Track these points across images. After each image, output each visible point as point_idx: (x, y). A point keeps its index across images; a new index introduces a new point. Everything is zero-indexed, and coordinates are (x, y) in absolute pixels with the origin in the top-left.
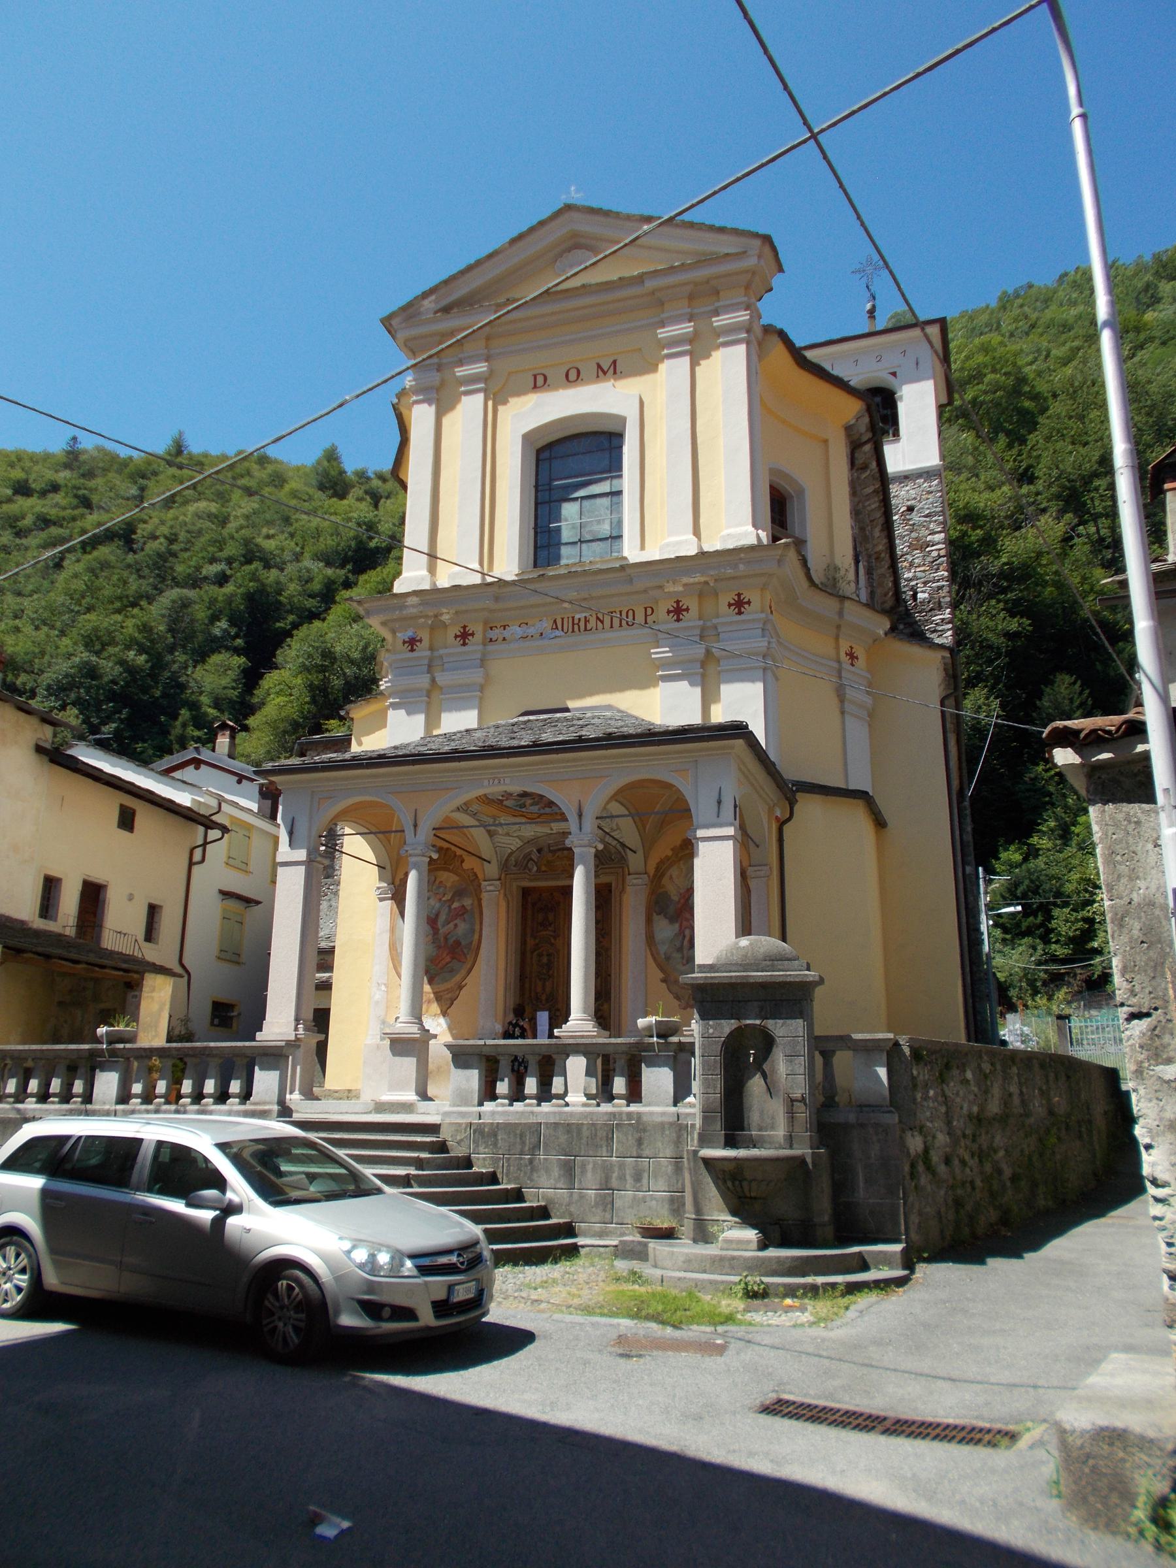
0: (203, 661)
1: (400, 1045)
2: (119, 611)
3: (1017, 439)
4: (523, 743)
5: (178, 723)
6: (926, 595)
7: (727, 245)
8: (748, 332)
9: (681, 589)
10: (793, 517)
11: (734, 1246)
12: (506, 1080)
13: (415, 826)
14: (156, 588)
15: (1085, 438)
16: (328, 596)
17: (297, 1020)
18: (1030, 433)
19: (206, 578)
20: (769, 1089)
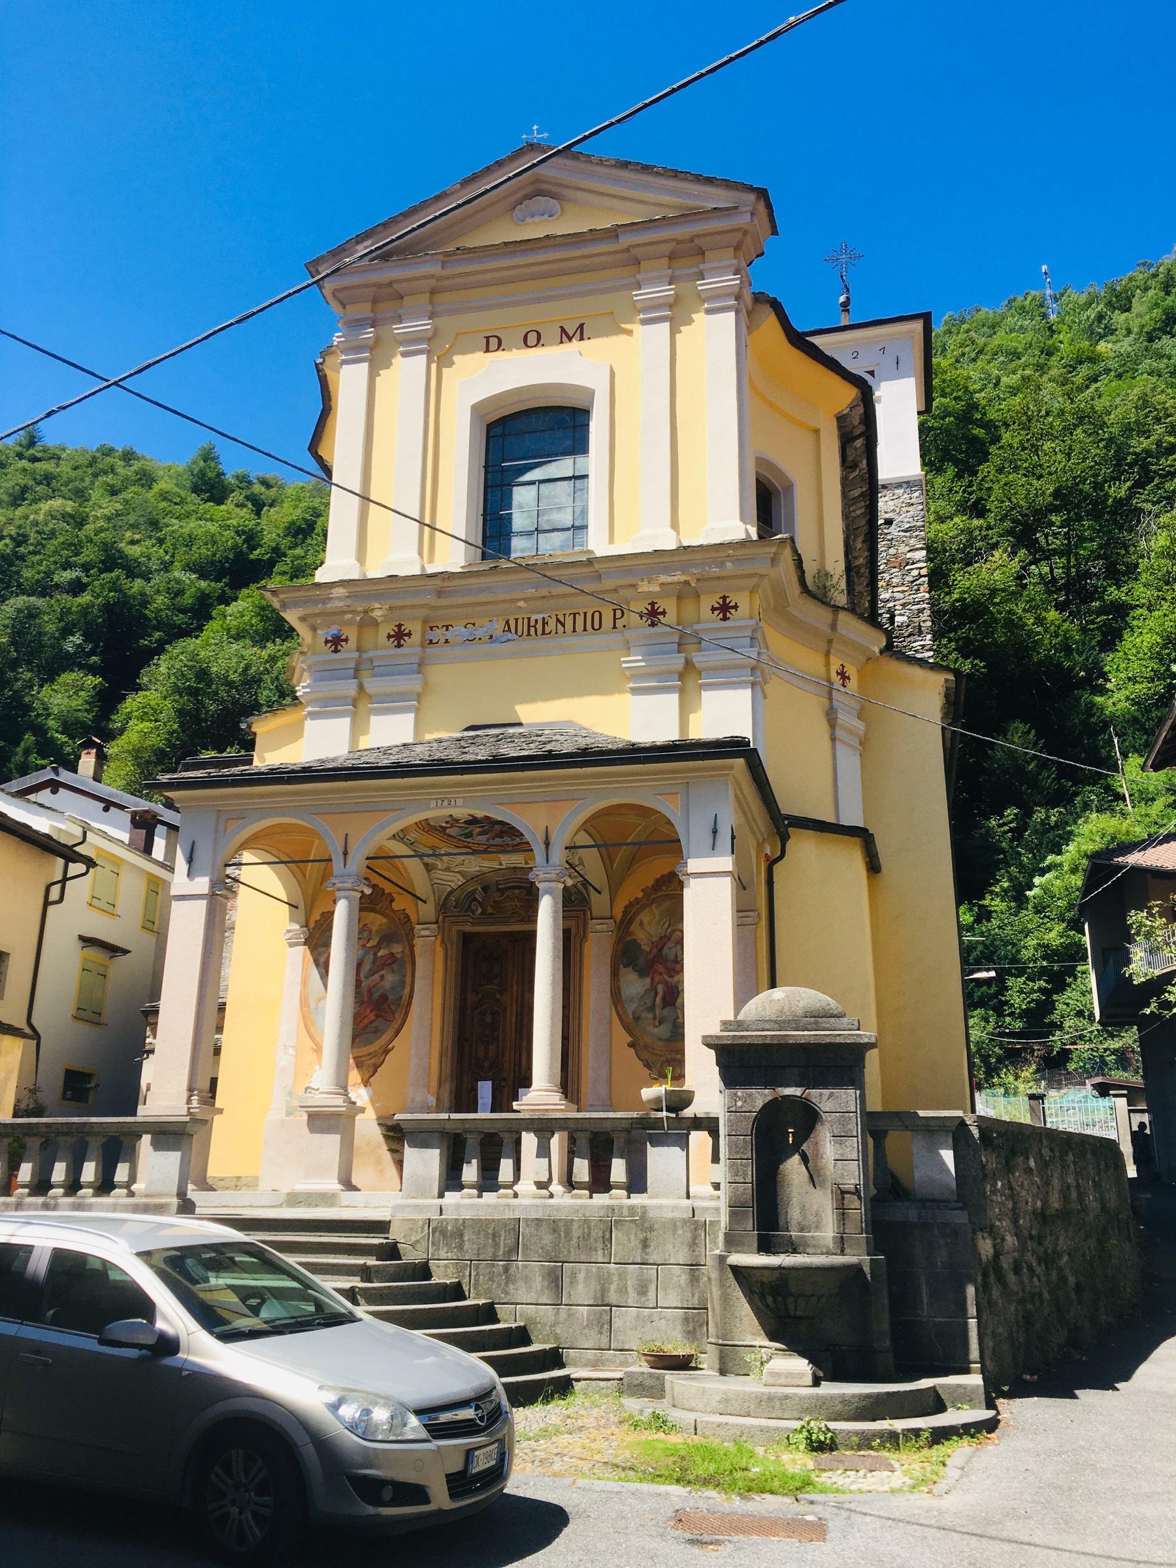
0: (52, 680)
1: (320, 1121)
3: (966, 469)
4: (479, 757)
5: (19, 750)
6: (905, 618)
7: (718, 198)
9: (657, 589)
11: (783, 1381)
12: (474, 1161)
13: (345, 853)
15: (1038, 471)
16: (201, 611)
17: (191, 1090)
18: (980, 464)
19: (57, 586)
20: (811, 1177)
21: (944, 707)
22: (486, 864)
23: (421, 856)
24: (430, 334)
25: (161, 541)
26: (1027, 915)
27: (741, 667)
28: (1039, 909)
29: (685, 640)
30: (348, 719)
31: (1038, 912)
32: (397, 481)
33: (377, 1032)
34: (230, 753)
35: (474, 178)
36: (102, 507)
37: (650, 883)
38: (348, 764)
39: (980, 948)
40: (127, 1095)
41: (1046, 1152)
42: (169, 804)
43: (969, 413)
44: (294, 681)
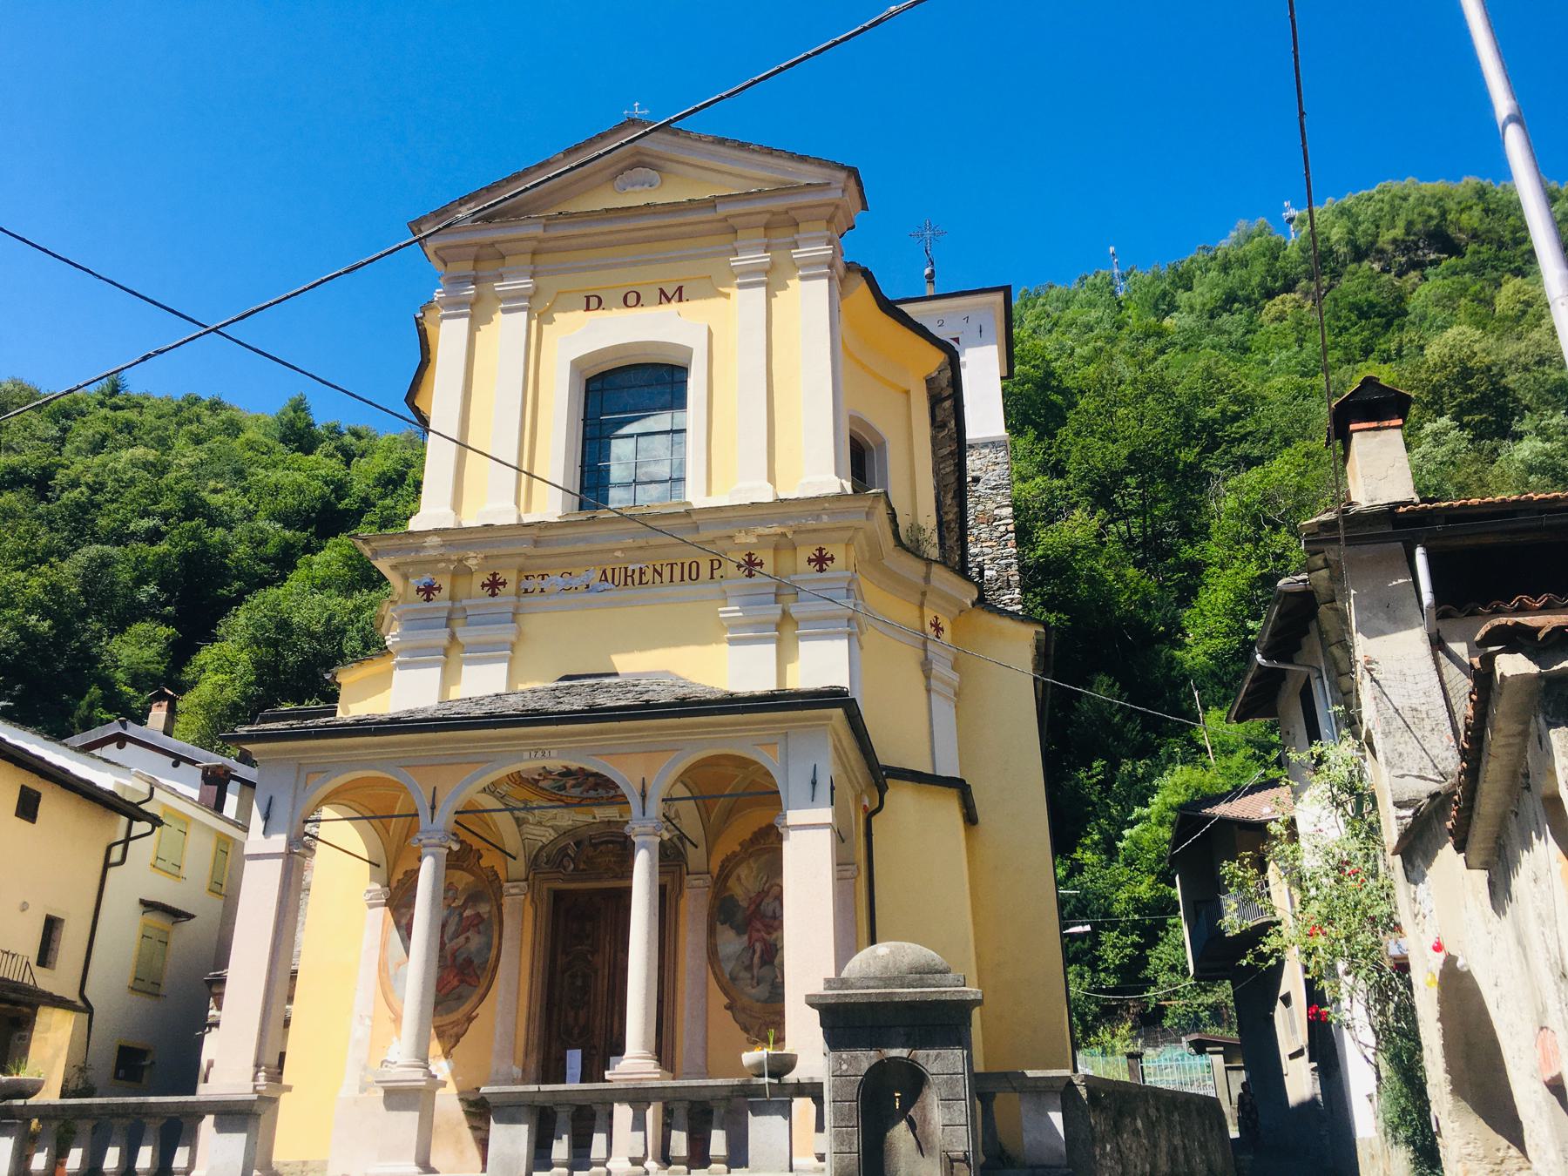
0: (122, 631)
1: (398, 1097)
2: (22, 568)
3: (1046, 432)
5: (83, 703)
7: (809, 174)
8: (830, 267)
10: (874, 468)
12: (565, 1137)
13: (433, 808)
14: (70, 543)
16: (285, 561)
17: (257, 1066)
19: (133, 533)
21: (1034, 659)
22: (580, 818)
23: (512, 810)
24: (531, 292)
25: (245, 491)
26: (1119, 869)
27: (840, 617)
28: (1129, 862)
29: (782, 590)
30: (438, 670)
31: (1128, 865)
32: (495, 428)
33: (461, 999)
34: (310, 705)
35: (577, 149)
36: (185, 455)
37: (748, 836)
38: (439, 714)
39: (1073, 901)
40: (187, 1073)
41: (1153, 1112)
42: (245, 758)
43: (1047, 381)
44: (383, 630)
